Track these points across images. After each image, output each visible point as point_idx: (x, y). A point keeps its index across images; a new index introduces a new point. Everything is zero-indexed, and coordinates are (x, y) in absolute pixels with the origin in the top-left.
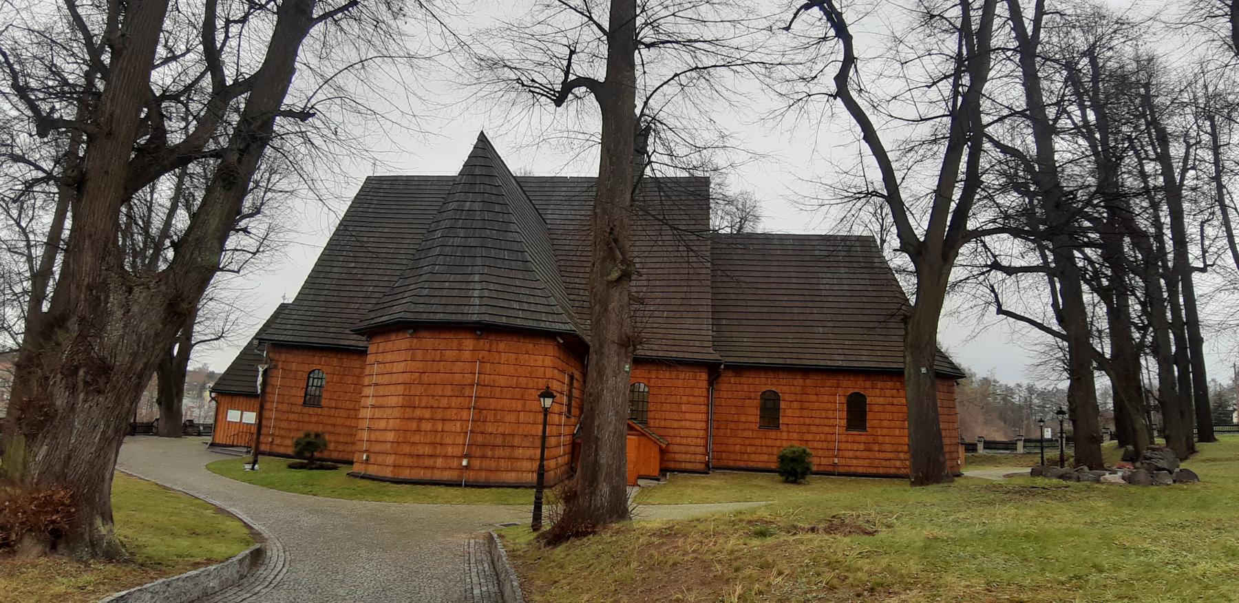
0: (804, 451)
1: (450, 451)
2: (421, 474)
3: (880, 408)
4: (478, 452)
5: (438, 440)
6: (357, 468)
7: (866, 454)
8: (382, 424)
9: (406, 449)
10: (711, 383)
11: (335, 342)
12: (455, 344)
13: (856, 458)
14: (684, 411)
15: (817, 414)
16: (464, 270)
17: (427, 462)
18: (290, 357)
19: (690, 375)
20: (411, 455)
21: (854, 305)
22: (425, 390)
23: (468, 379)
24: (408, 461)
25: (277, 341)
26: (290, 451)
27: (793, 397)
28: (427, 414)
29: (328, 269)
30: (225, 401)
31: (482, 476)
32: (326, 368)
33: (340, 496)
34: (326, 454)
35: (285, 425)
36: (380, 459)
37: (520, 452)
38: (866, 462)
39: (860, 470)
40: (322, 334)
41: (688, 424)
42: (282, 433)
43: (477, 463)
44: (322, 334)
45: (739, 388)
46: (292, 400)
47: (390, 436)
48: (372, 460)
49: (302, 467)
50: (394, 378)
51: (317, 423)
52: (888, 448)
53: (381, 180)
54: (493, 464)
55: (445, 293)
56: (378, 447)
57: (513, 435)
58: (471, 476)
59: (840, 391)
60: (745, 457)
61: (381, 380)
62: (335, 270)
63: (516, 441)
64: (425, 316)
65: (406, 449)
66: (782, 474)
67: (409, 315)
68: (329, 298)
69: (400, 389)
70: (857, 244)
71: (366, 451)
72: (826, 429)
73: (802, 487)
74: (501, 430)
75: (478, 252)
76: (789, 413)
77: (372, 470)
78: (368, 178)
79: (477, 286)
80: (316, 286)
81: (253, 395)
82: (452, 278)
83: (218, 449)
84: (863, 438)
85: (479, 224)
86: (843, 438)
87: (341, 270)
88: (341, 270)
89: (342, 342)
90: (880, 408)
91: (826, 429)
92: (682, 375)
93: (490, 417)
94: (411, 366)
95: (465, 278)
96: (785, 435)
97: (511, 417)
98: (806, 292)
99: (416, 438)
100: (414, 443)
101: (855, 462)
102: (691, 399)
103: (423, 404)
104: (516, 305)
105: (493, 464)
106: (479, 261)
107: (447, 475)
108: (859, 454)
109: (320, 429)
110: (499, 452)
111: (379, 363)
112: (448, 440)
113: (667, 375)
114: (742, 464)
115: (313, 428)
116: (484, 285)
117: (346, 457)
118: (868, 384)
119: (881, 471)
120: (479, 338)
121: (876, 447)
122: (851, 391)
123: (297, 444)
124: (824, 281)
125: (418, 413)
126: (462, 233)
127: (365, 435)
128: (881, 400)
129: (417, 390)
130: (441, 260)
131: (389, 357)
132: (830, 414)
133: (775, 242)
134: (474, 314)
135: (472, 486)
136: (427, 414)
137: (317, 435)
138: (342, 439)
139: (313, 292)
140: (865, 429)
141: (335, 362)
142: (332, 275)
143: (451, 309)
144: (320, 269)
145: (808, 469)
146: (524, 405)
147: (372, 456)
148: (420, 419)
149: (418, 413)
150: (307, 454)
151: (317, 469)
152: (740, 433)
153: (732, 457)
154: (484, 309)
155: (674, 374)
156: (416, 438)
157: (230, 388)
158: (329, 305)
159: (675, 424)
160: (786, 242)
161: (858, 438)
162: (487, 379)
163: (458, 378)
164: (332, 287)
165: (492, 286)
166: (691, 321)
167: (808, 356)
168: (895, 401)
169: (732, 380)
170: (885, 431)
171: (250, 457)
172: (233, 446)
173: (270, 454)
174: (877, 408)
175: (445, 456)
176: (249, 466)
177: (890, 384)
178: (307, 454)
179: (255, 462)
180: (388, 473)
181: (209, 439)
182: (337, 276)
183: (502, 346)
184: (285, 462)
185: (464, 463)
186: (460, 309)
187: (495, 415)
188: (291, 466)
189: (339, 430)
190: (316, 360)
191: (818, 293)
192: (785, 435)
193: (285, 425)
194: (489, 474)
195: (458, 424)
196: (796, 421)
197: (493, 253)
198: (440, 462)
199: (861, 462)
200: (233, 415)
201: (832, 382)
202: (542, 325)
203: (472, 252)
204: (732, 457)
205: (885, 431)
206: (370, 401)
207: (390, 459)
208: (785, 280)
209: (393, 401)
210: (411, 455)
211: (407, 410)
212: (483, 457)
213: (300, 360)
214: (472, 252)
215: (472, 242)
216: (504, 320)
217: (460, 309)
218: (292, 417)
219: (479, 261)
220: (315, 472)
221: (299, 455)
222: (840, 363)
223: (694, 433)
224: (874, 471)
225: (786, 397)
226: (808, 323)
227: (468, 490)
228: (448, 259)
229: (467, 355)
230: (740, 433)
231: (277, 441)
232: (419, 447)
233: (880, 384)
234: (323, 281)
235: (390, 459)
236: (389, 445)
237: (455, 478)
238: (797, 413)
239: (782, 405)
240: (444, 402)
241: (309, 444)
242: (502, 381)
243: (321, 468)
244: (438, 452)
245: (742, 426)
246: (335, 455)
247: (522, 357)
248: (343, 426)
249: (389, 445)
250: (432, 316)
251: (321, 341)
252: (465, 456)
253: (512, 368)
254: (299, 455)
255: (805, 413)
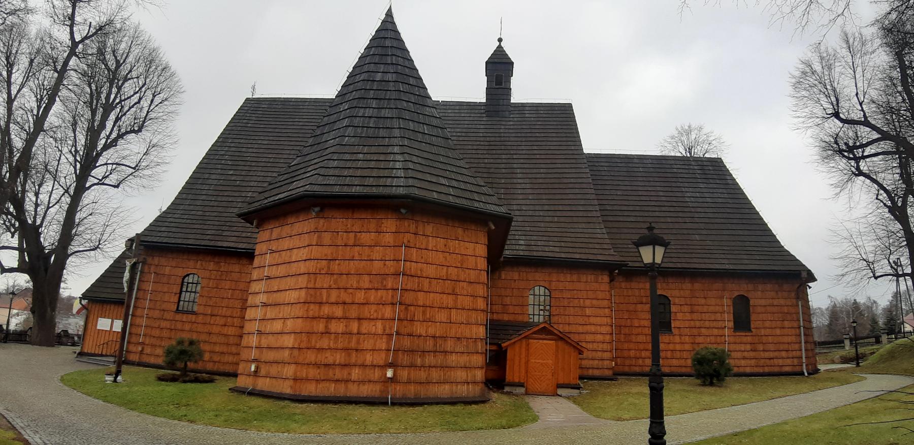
0: (724, 351)
1: (369, 358)
2: (331, 389)
3: (763, 309)
4: (404, 359)
5: (353, 345)
6: (242, 382)
7: (752, 354)
8: (277, 326)
9: (311, 357)
10: (611, 281)
11: (212, 243)
12: (372, 226)
13: (744, 358)
14: (596, 314)
15: (707, 316)
16: (380, 141)
17: (339, 373)
18: (163, 261)
19: (591, 278)
20: (317, 365)
21: (720, 215)
22: (335, 282)
23: (391, 267)
24: (313, 372)
25: (147, 247)
26: (160, 361)
27: (682, 301)
28: (338, 311)
29: (207, 176)
30: (96, 308)
31: (412, 391)
32: (199, 274)
33: (228, 423)
34: (200, 366)
35: (156, 333)
36: (274, 370)
37: (453, 359)
38: (753, 362)
39: (748, 370)
40: (198, 237)
41: (593, 329)
42: (153, 341)
43: (404, 374)
44: (198, 237)
45: (630, 293)
46: (164, 306)
47: (289, 341)
48: (263, 372)
49: (174, 379)
50: (294, 269)
51: (190, 331)
52: (771, 347)
53: (259, 101)
54: (422, 375)
55: (360, 164)
56: (271, 356)
57: (444, 338)
58: (398, 391)
59: (726, 294)
60: (640, 361)
61: (274, 272)
62: (213, 177)
63: (449, 345)
64: (337, 189)
65: (311, 357)
66: (698, 376)
67: (316, 188)
68: (206, 203)
69: (302, 281)
70: (709, 163)
71: (254, 361)
72: (716, 332)
73: (722, 389)
74: (431, 331)
75: (396, 123)
76: (680, 318)
77: (263, 384)
78: (247, 99)
79: (399, 157)
80: (193, 192)
81: (119, 303)
82: (366, 150)
83: (85, 359)
84: (749, 339)
85: (394, 95)
86: (732, 339)
87: (218, 177)
88: (218, 177)
89: (219, 244)
90: (763, 309)
91: (716, 332)
92: (584, 278)
93: (419, 315)
94: (316, 252)
95: (382, 149)
96: (677, 339)
97: (442, 316)
98: (674, 204)
99: (324, 343)
100: (321, 350)
101: (743, 362)
102: (594, 302)
103: (333, 299)
104: (443, 181)
105: (422, 375)
106: (397, 133)
107: (366, 391)
108: (746, 354)
109: (194, 337)
110: (430, 360)
111: (273, 252)
112: (368, 344)
113: (568, 277)
114: (637, 369)
115: (186, 336)
116: (407, 157)
117: (229, 369)
118: (751, 287)
119: (767, 370)
120: (402, 218)
121: (761, 347)
122: (736, 294)
123: (169, 352)
124: (689, 195)
125: (326, 310)
126: (374, 104)
127: (253, 341)
128: (763, 302)
129: (325, 281)
130: (350, 131)
131: (286, 244)
132: (718, 316)
133: (636, 161)
134: (399, 186)
135: (401, 404)
136: (338, 311)
137: (192, 343)
138: (217, 349)
139: (190, 196)
140: (750, 330)
141: (211, 266)
142: (210, 182)
143: (371, 181)
144: (198, 175)
145: (729, 370)
146: (456, 301)
147: (262, 366)
148: (329, 318)
149: (326, 310)
150: (180, 365)
151: (191, 381)
152: (633, 338)
153: (627, 362)
154: (411, 182)
155: (575, 277)
156: (324, 343)
157: (100, 296)
158: (207, 209)
159: (581, 329)
160: (645, 161)
161: (745, 339)
162: (413, 267)
163: (377, 266)
164: (210, 192)
165: (415, 159)
166: (584, 225)
167: (695, 260)
168: (776, 302)
169: (623, 285)
170: (768, 332)
171: (113, 368)
172: (102, 355)
173: (140, 364)
174: (759, 309)
175: (363, 366)
176: (109, 379)
177: (769, 286)
178: (180, 365)
179: (118, 373)
180: (286, 388)
181: (78, 349)
182: (215, 182)
183: (429, 229)
184: (153, 373)
185: (390, 374)
186: (382, 181)
187: (424, 313)
188: (161, 379)
189: (214, 339)
190: (191, 263)
191: (685, 205)
192: (677, 339)
193: (156, 333)
194: (419, 387)
195: (379, 324)
196: (687, 324)
197: (411, 125)
198: (356, 373)
199: (749, 362)
200: (104, 324)
201: (718, 285)
202: (476, 205)
203: (388, 123)
204: (627, 362)
205: (768, 332)
206: (262, 298)
207: (289, 371)
208: (653, 193)
209: (293, 296)
210: (317, 365)
211: (312, 306)
212: (412, 366)
213: (174, 264)
214: (388, 123)
215: (386, 113)
216: (435, 195)
217: (382, 181)
218: (164, 324)
219: (397, 133)
220: (189, 385)
221: (171, 365)
222: (727, 267)
223: (599, 338)
224: (761, 370)
225: (677, 301)
226: (685, 232)
227: (399, 410)
228: (359, 130)
229: (388, 238)
230: (633, 338)
231: (148, 350)
232: (328, 354)
233: (760, 287)
234: (199, 187)
235: (289, 371)
236: (287, 353)
237: (377, 394)
238: (688, 316)
239: (673, 309)
240: (360, 296)
241: (183, 352)
242: (431, 271)
243: (197, 380)
244: (353, 360)
245: (635, 331)
246: (210, 367)
247: (451, 243)
248: (219, 334)
249: (287, 353)
250: (346, 190)
251: (198, 242)
252: (390, 365)
253: (441, 255)
254: (171, 365)
255: (695, 316)
